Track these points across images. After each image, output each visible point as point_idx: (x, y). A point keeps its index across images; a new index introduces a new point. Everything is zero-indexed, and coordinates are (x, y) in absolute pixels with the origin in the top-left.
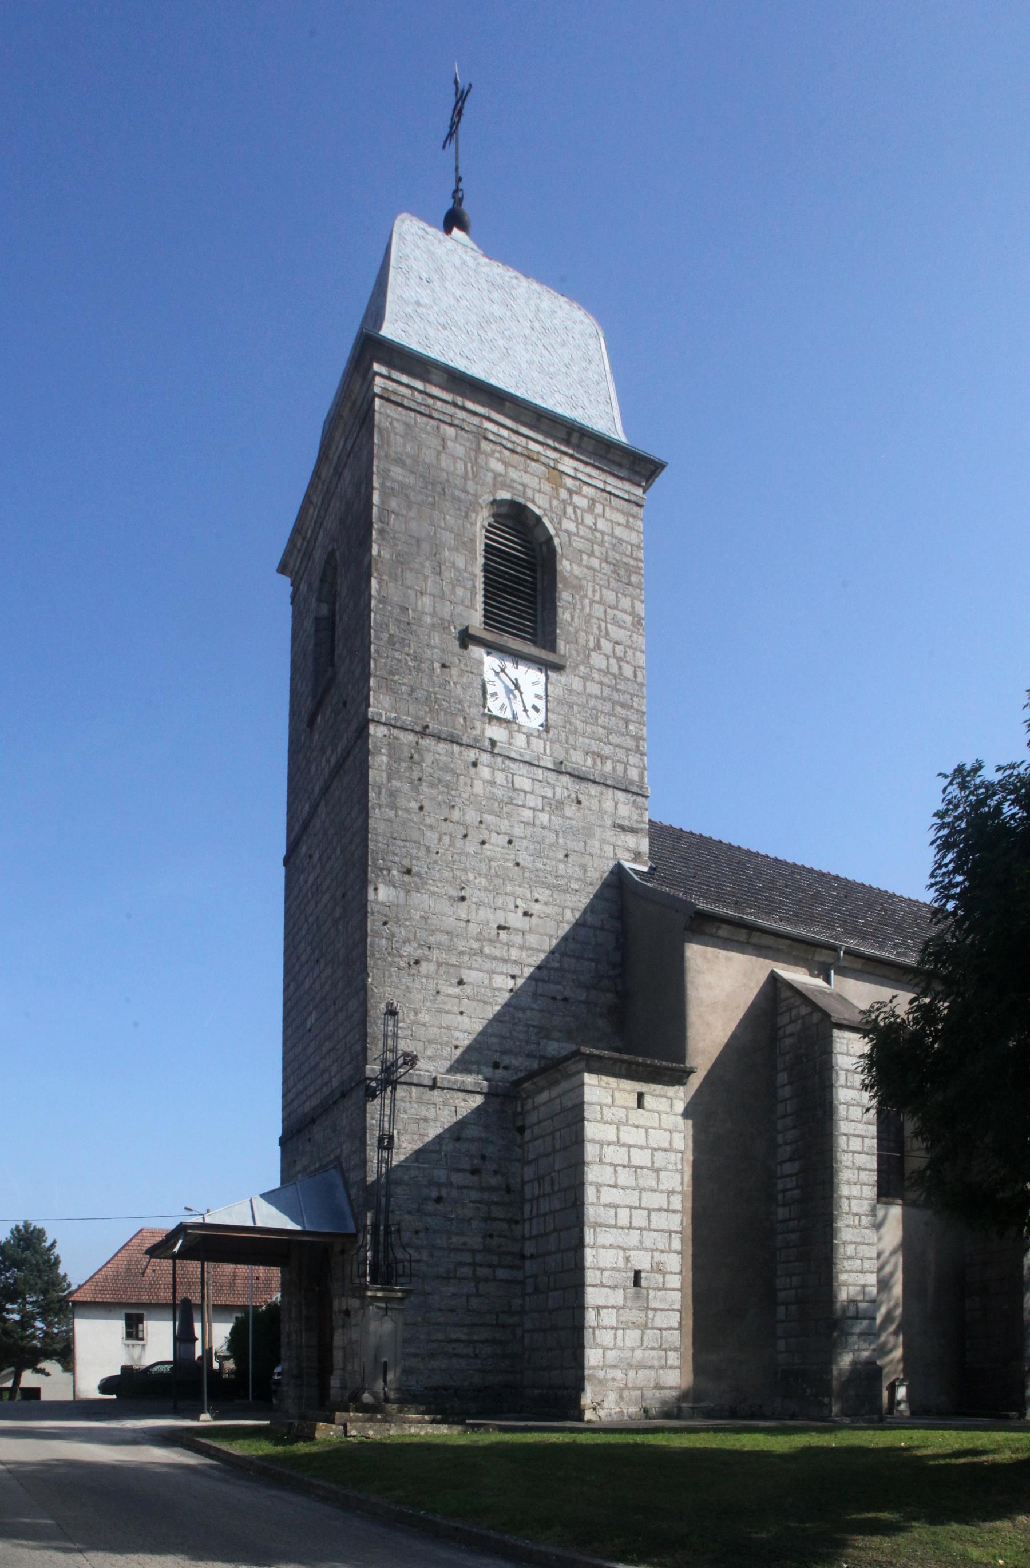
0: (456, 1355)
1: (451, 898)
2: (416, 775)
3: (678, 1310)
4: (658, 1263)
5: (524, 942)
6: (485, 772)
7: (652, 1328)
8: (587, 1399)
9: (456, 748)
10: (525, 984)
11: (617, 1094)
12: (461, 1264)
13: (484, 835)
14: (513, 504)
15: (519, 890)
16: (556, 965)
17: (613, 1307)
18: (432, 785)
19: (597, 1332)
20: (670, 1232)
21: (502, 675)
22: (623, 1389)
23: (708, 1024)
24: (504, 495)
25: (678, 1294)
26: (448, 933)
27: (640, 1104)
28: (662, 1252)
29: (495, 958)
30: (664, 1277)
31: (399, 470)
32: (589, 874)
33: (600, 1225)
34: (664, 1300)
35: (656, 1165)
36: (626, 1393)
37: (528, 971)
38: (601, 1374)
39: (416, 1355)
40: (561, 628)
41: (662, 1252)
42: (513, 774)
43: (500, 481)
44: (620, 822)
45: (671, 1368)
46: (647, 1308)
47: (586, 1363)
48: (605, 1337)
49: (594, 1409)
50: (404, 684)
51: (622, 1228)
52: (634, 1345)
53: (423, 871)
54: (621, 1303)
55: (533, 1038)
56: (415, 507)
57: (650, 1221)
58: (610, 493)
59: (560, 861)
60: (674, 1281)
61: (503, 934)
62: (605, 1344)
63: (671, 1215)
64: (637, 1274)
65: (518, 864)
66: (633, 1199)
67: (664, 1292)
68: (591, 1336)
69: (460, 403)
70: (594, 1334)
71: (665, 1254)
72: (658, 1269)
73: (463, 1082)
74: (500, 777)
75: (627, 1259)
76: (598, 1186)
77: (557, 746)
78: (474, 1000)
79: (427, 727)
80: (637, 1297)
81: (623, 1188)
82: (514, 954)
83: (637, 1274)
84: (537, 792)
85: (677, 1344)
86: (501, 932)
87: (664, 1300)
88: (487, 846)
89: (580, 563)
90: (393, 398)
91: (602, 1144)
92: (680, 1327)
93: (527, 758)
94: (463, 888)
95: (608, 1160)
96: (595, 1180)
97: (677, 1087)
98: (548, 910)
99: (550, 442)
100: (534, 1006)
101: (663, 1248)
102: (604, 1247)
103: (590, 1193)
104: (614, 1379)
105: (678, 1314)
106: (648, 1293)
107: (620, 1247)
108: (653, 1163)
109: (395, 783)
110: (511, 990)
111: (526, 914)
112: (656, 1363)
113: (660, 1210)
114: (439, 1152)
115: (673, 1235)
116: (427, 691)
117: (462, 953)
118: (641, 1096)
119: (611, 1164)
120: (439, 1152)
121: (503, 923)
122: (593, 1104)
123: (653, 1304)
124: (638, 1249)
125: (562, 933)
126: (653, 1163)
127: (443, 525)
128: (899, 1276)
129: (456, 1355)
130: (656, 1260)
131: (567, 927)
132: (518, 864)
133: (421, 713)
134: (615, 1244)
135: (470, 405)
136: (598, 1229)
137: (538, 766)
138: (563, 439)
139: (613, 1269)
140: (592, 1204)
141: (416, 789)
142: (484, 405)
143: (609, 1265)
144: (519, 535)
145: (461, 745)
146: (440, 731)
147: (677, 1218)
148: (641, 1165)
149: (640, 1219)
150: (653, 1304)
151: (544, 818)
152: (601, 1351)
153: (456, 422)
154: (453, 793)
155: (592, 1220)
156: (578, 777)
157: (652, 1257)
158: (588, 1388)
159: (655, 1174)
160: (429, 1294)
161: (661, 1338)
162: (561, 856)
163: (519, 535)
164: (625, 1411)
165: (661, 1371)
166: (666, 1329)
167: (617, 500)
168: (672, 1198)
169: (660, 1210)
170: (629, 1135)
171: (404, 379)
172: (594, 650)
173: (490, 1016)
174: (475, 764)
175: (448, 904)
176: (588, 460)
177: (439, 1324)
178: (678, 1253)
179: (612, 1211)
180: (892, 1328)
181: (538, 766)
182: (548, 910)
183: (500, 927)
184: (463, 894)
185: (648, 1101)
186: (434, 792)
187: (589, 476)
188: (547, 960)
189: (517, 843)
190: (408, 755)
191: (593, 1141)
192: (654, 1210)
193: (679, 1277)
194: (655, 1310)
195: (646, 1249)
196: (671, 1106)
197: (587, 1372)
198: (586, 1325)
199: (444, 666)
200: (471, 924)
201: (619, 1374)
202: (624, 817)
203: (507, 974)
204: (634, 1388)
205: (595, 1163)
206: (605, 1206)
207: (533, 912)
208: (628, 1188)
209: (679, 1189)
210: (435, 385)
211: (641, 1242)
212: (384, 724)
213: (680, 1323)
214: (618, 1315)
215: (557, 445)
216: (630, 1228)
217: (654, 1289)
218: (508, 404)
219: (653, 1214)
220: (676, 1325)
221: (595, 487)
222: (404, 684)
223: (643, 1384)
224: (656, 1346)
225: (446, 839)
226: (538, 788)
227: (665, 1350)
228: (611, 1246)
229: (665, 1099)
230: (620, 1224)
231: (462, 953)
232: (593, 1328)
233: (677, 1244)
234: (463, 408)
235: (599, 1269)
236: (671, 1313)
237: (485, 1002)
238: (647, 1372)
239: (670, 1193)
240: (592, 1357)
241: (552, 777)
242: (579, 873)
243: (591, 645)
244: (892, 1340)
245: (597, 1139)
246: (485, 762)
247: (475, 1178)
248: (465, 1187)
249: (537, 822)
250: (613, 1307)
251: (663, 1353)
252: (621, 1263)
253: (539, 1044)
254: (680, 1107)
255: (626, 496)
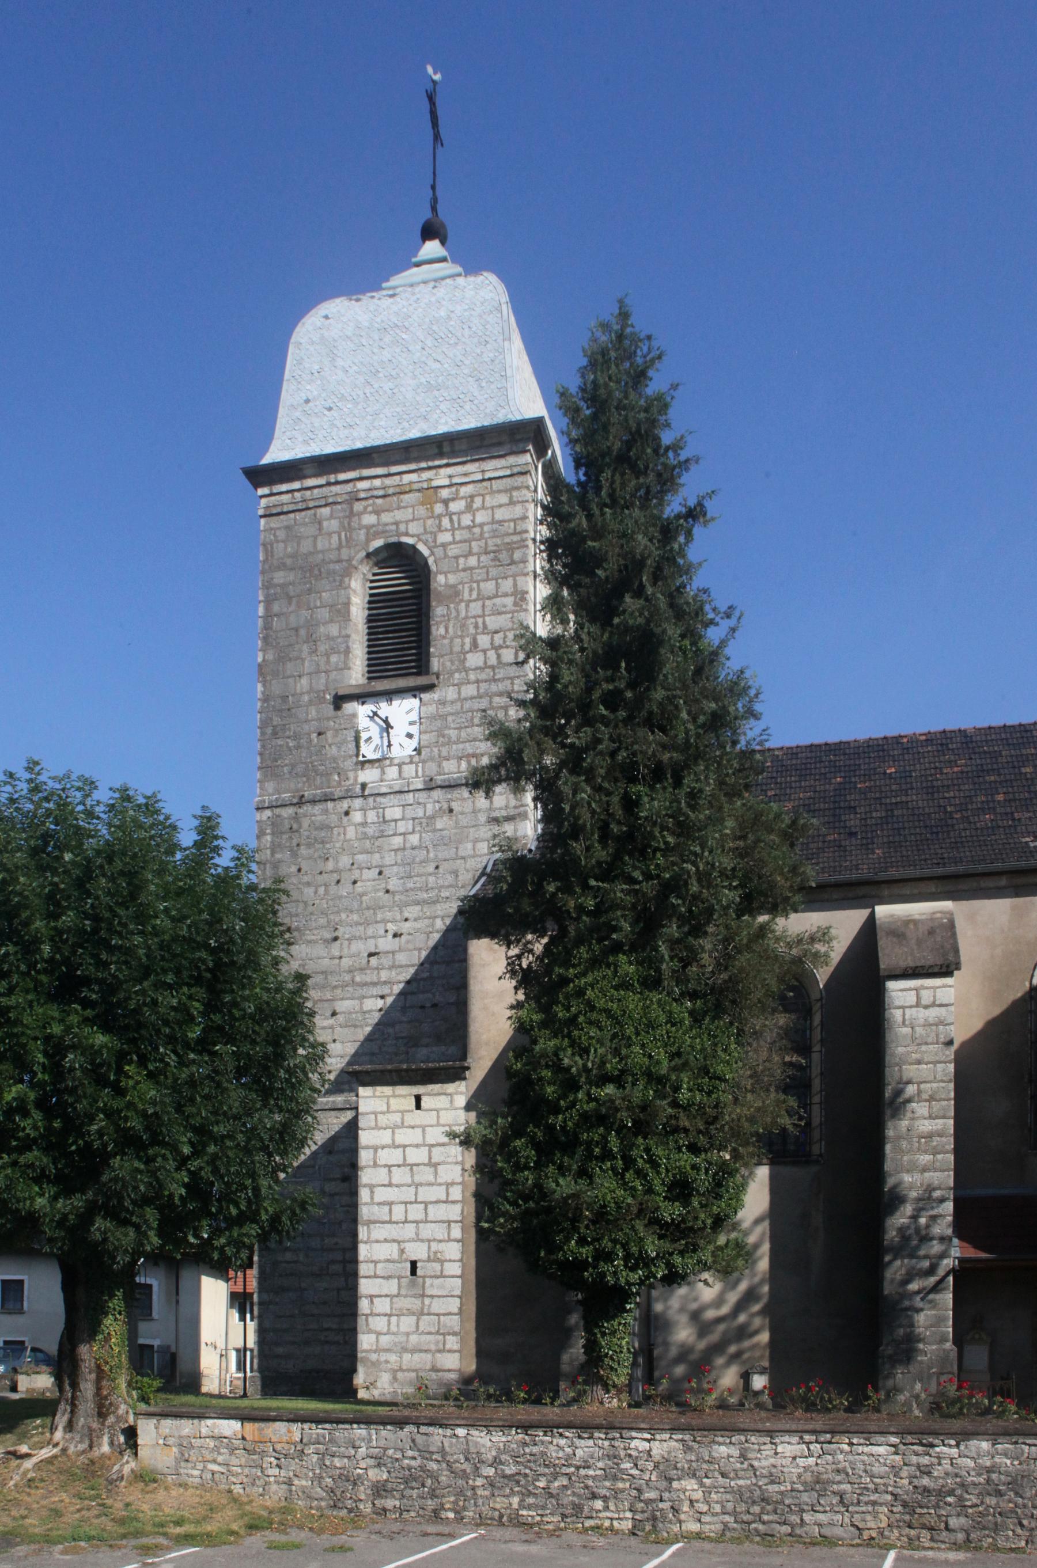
0: (327, 1342)
1: (326, 941)
2: (295, 842)
3: (458, 1296)
4: (435, 1253)
5: (394, 962)
6: (357, 817)
7: (429, 1314)
8: (360, 1378)
9: (330, 805)
10: (394, 1001)
11: (392, 1101)
12: (333, 1262)
13: (356, 874)
14: (388, 546)
15: (389, 915)
16: (426, 975)
17: (386, 1296)
18: (309, 846)
19: (370, 1319)
20: (449, 1222)
21: (376, 718)
22: (397, 1371)
23: (493, 1014)
24: (378, 543)
25: (459, 1281)
26: (322, 973)
27: (418, 1107)
28: (440, 1241)
29: (365, 984)
30: (442, 1266)
31: (281, 574)
32: (460, 878)
33: (375, 1222)
34: (442, 1287)
35: (433, 1161)
36: (400, 1375)
37: (397, 988)
38: (374, 1357)
39: (293, 1343)
40: (435, 646)
41: (440, 1241)
42: (384, 808)
43: (372, 532)
44: (497, 814)
45: (449, 1351)
46: (423, 1296)
47: (359, 1346)
48: (379, 1324)
49: (367, 1388)
50: (286, 765)
51: (397, 1223)
52: (408, 1330)
53: (301, 925)
54: (395, 1291)
55: (403, 1048)
56: (294, 601)
57: (426, 1214)
58: (490, 479)
59: (430, 874)
60: (455, 1269)
61: (374, 961)
62: (378, 1329)
63: (450, 1206)
64: (414, 1265)
65: (388, 891)
66: (409, 1194)
67: (441, 1280)
68: (364, 1322)
69: (333, 480)
70: (367, 1320)
71: (443, 1244)
72: (435, 1258)
73: (334, 1102)
74: (372, 816)
75: (402, 1251)
76: (372, 1187)
77: (429, 764)
78: (346, 1026)
79: (303, 796)
80: (413, 1285)
81: (397, 1186)
82: (384, 975)
83: (414, 1265)
84: (408, 816)
85: (457, 1329)
86: (371, 959)
87: (442, 1287)
88: (359, 884)
89: (457, 570)
90: (274, 511)
91: (376, 1149)
92: (460, 1313)
93: (397, 789)
94: (336, 929)
95: (383, 1162)
96: (368, 1182)
97: (457, 1083)
98: (418, 925)
99: (423, 465)
100: (404, 1019)
101: (441, 1238)
102: (377, 1241)
103: (364, 1195)
104: (387, 1362)
105: (458, 1300)
106: (424, 1283)
107: (394, 1241)
108: (430, 1158)
109: (278, 856)
110: (380, 1010)
111: (395, 935)
112: (433, 1347)
113: (437, 1202)
114: (313, 1167)
115: (453, 1225)
116: (305, 763)
117: (335, 987)
118: (418, 1099)
119: (385, 1166)
120: (313, 1167)
121: (373, 950)
122: (367, 1114)
123: (429, 1292)
124: (413, 1240)
125: (431, 943)
126: (430, 1158)
127: (318, 604)
128: (766, 1247)
129: (327, 1342)
130: (433, 1249)
131: (436, 937)
132: (388, 891)
133: (300, 785)
134: (389, 1238)
135: (342, 477)
136: (372, 1226)
137: (409, 791)
138: (436, 455)
139: (388, 1261)
140: (366, 1204)
141: (295, 854)
142: (354, 469)
143: (382, 1258)
144: (404, 568)
145: (334, 800)
146: (315, 795)
147: (458, 1208)
148: (417, 1162)
149: (416, 1212)
150: (428, 1292)
151: (414, 839)
152: (374, 1336)
153: (330, 500)
154: (328, 846)
155: (365, 1218)
156: (450, 786)
157: (429, 1248)
158: (361, 1370)
159: (432, 1169)
160: (305, 1289)
161: (439, 1322)
162: (431, 868)
163: (404, 568)
164: (399, 1391)
165: (439, 1355)
166: (444, 1315)
167: (499, 481)
168: (451, 1190)
169: (437, 1202)
170: (404, 1136)
171: (284, 487)
172: (470, 651)
173: (362, 1038)
174: (347, 813)
175: (322, 946)
176: (464, 459)
177: (313, 1315)
178: (458, 1241)
179: (386, 1208)
180: (756, 1308)
181: (409, 791)
182: (418, 925)
183: (371, 955)
184: (336, 934)
185: (425, 1102)
186: (311, 851)
187: (465, 475)
188: (416, 973)
189: (387, 872)
190: (288, 826)
191: (367, 1147)
192: (431, 1203)
193: (459, 1264)
194: (432, 1297)
195: (422, 1241)
196: (451, 1102)
197: (359, 1355)
198: (360, 1312)
199: (320, 734)
200: (343, 960)
201: (393, 1358)
202: (501, 809)
203: (376, 996)
204: (408, 1370)
205: (369, 1166)
206: (379, 1204)
207: (404, 931)
208: (402, 1185)
209: (459, 1180)
210: (310, 477)
211: (417, 1234)
212: (268, 808)
213: (460, 1309)
214: (392, 1303)
215: (430, 464)
216: (406, 1222)
217: (431, 1277)
218: (374, 455)
219: (430, 1207)
220: (456, 1310)
221: (473, 482)
222: (286, 765)
223: (418, 1366)
224: (433, 1330)
225: (321, 890)
226: (410, 812)
227: (444, 1334)
228: (386, 1241)
229: (444, 1097)
230: (394, 1219)
231: (335, 987)
232: (367, 1315)
233: (457, 1232)
234: (337, 483)
235: (372, 1262)
236: (449, 1299)
237: (355, 1026)
238: (423, 1355)
239: (449, 1185)
240: (365, 1341)
241: (422, 796)
242: (450, 879)
243: (467, 647)
244: (757, 1322)
245: (370, 1144)
246: (357, 807)
247: (346, 1184)
248: (336, 1194)
249: (408, 845)
250: (386, 1296)
251: (441, 1337)
252: (395, 1255)
253: (407, 1053)
254: (461, 1101)
255: (508, 472)
